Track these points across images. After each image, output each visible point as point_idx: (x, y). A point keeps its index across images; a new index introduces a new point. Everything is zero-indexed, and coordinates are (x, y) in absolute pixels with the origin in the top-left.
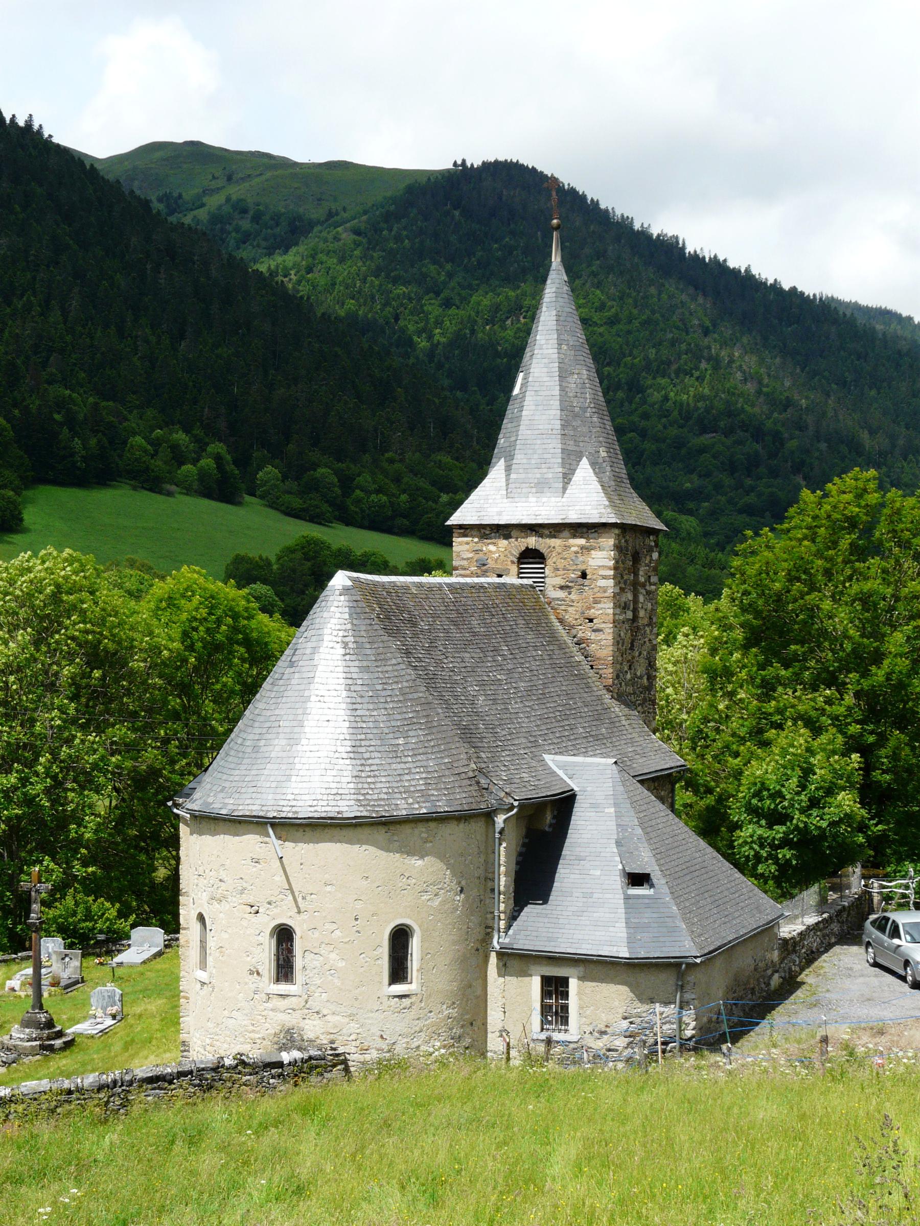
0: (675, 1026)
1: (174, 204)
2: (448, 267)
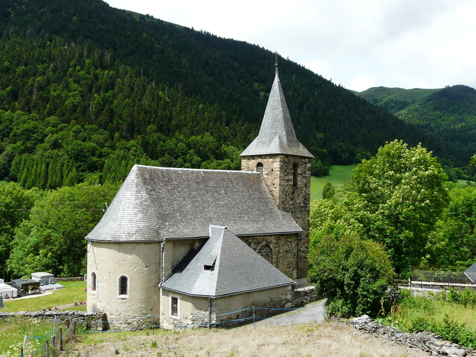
0: (208, 319)
1: (376, 101)
2: (443, 111)
